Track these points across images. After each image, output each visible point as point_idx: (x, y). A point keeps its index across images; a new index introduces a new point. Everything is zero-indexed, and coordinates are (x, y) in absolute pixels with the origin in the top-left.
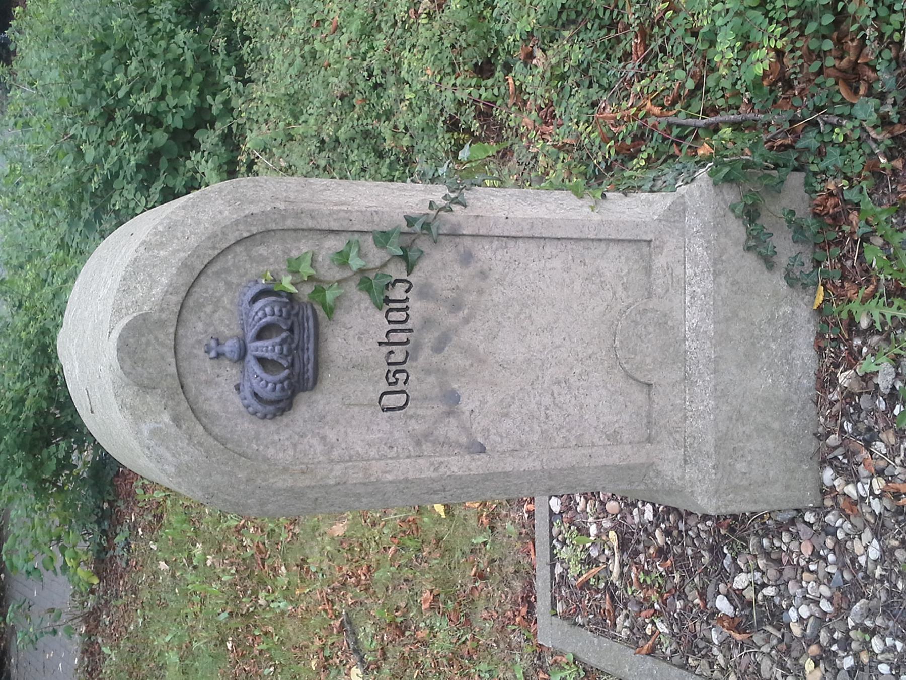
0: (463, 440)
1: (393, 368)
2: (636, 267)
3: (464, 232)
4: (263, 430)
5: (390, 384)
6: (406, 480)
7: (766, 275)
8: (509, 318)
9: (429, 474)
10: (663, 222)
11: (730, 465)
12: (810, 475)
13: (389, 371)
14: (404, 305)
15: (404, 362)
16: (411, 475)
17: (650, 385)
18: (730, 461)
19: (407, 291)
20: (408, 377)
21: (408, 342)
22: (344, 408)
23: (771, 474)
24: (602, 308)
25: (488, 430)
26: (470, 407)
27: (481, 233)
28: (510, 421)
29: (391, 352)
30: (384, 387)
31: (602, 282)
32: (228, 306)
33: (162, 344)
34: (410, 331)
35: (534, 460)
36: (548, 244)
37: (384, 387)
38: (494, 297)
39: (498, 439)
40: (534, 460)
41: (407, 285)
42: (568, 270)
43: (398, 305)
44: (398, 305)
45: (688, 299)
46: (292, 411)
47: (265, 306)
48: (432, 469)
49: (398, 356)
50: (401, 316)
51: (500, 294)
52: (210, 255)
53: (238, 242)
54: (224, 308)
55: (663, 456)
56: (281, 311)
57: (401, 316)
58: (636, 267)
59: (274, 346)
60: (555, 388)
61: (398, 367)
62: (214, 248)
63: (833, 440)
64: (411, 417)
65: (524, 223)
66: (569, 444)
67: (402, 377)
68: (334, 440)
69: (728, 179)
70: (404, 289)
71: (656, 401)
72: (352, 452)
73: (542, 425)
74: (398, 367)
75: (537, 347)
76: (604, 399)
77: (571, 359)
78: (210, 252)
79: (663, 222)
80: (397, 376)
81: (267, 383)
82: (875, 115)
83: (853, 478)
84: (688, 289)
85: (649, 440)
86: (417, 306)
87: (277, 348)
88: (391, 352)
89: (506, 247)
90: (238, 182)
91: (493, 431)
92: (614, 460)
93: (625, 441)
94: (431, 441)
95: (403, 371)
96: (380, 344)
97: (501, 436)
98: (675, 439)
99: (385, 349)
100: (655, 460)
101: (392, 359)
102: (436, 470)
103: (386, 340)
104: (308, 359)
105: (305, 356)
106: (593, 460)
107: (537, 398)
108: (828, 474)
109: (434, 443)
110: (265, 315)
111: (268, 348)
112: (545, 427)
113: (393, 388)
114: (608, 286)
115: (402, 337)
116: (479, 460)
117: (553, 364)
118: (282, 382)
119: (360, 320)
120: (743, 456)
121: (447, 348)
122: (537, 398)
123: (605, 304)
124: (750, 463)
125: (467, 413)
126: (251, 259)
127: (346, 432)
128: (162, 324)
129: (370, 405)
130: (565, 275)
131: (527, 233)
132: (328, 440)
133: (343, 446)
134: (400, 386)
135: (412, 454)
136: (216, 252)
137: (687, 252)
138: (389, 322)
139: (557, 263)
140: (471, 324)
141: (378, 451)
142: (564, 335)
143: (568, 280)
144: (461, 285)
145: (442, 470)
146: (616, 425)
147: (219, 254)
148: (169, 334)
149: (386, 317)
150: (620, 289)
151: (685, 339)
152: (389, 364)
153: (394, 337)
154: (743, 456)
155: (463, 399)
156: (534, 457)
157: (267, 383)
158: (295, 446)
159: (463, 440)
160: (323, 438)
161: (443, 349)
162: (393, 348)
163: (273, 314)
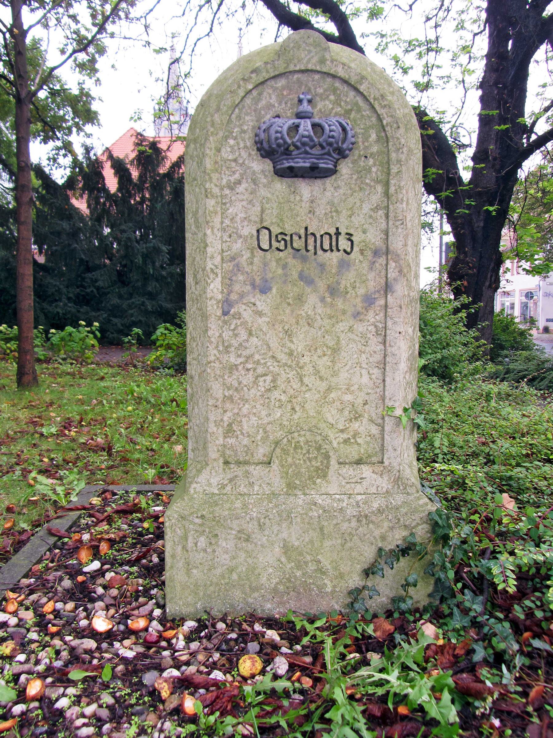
0: (234, 297)
1: (288, 238)
2: (362, 451)
3: (389, 296)
4: (247, 136)
5: (277, 236)
6: (207, 245)
7: (359, 568)
8: (324, 337)
9: (209, 265)
10: (398, 474)
11: (204, 531)
12: (191, 609)
13: (286, 235)
14: (334, 248)
15: (293, 248)
16: (209, 250)
17: (270, 463)
18: (207, 530)
19: (345, 251)
20: (281, 251)
21: (307, 251)
22: (261, 199)
23: (195, 571)
24: (330, 420)
25: (240, 318)
26: (258, 303)
27: (389, 310)
28: (245, 338)
29: (300, 237)
30: (275, 230)
31: (351, 420)
32: (334, 111)
33: (309, 61)
34: (315, 253)
35: (215, 355)
36: (380, 371)
37: (275, 230)
38: (340, 324)
39: (232, 327)
40: (215, 355)
41: (349, 250)
42: (360, 389)
43: (334, 244)
44: (334, 244)
45: (337, 496)
46: (260, 158)
47: (336, 126)
48: (213, 267)
49: (298, 243)
50: (326, 246)
51: (342, 329)
52: (370, 96)
53: (378, 115)
54: (333, 109)
55: (214, 474)
56: (333, 137)
57: (326, 246)
58: (362, 451)
59: (308, 131)
60: (269, 378)
61: (289, 243)
62: (375, 99)
63: (221, 626)
64: (252, 253)
65: (396, 348)
66: (226, 389)
67: (282, 245)
68: (238, 191)
69: (435, 525)
70: (346, 248)
71: (257, 468)
72: (228, 205)
73: (242, 365)
74: (289, 243)
75: (302, 362)
76: (260, 422)
77: (292, 392)
78: (372, 96)
79: (398, 474)
80: (283, 242)
81: (281, 127)
82: (504, 623)
83: (189, 639)
84: (345, 497)
85: (226, 463)
86: (334, 257)
87: (306, 133)
88: (300, 237)
89: (378, 334)
90: (417, 130)
91: (239, 322)
92: (212, 428)
93: (226, 440)
94: (233, 269)
95: (286, 247)
96: (306, 228)
97: (234, 330)
98: (226, 485)
99: (302, 232)
100: (210, 466)
101: (295, 238)
102: (212, 270)
103: (309, 233)
104: (297, 163)
105: (300, 160)
106: (213, 409)
107: (262, 361)
108: (191, 624)
109: (231, 271)
110: (329, 126)
111: (306, 126)
112: (240, 368)
113: (273, 239)
114: (348, 425)
115: (311, 247)
116: (218, 307)
117: (289, 376)
118: (282, 138)
119: (323, 212)
120: (210, 543)
121: (302, 283)
122: (262, 361)
123: (334, 423)
124: (205, 551)
125: (253, 300)
126: (367, 129)
127: (243, 200)
128: (322, 61)
129: (262, 221)
130: (356, 386)
131: (389, 349)
132: (238, 186)
133: (233, 198)
134: (275, 244)
135: (224, 254)
136: (372, 101)
137: (374, 496)
138: (322, 236)
139: (365, 379)
140: (320, 304)
141: (228, 226)
142: (310, 385)
143: (352, 388)
144: (348, 296)
145: (212, 276)
146: (239, 433)
147: (371, 103)
148: (316, 66)
149: (326, 233)
150: (345, 436)
151: (305, 494)
152: (291, 235)
153: (311, 240)
154: (210, 543)
155: (264, 297)
156: (218, 356)
157: (281, 127)
158: (235, 160)
159: (234, 297)
160: (239, 182)
161: (302, 280)
162: (303, 239)
163: (331, 131)
